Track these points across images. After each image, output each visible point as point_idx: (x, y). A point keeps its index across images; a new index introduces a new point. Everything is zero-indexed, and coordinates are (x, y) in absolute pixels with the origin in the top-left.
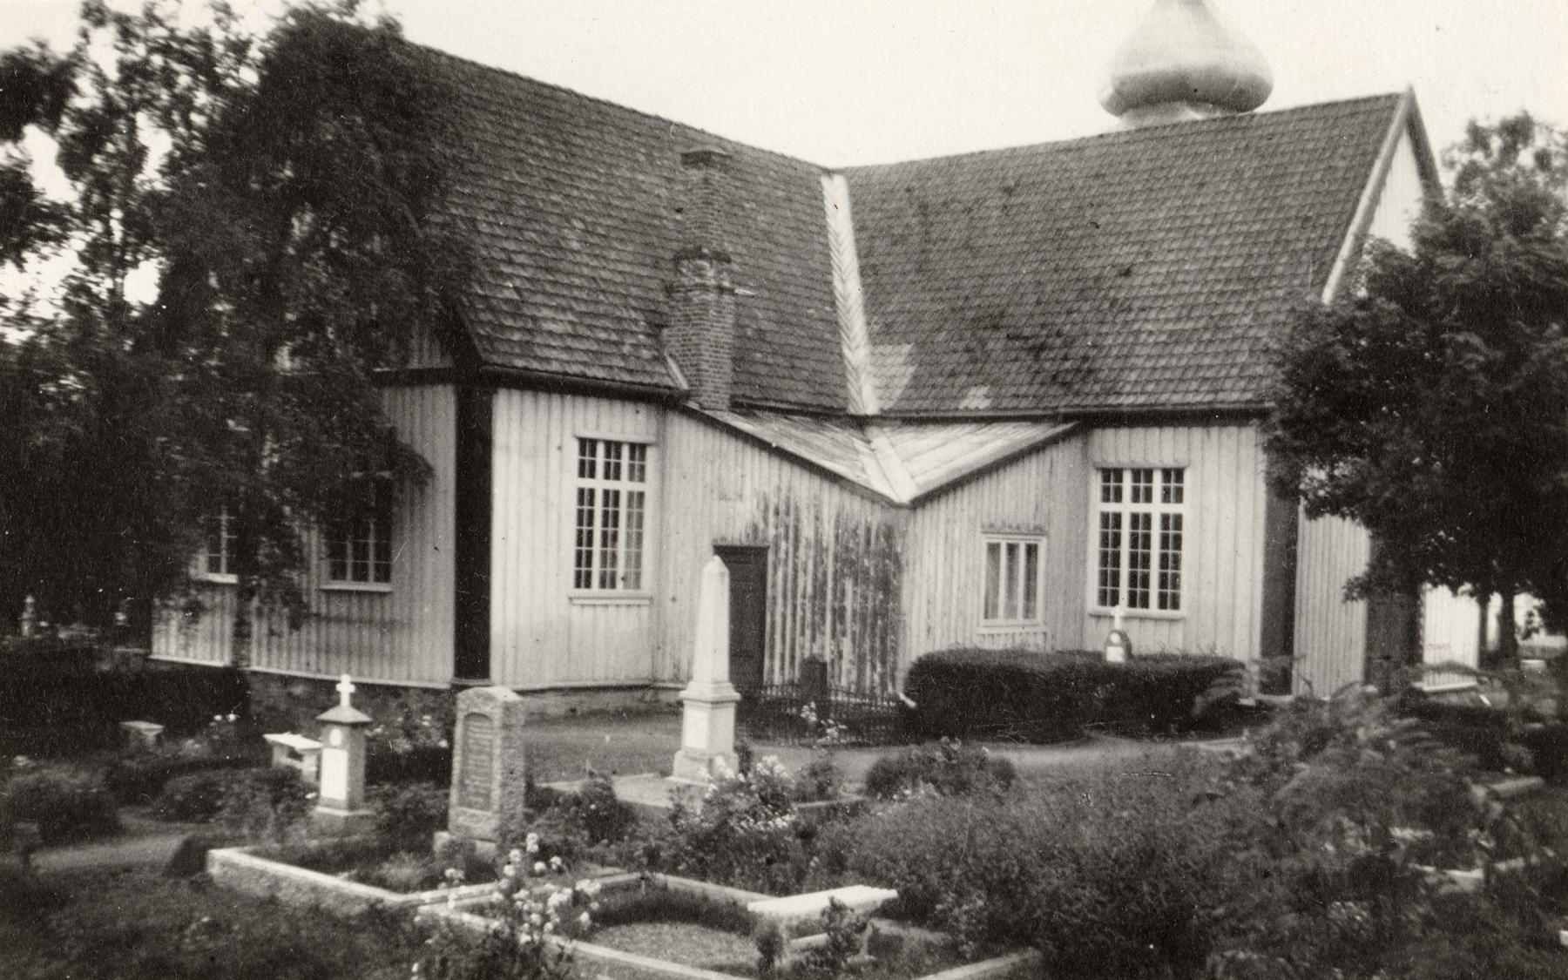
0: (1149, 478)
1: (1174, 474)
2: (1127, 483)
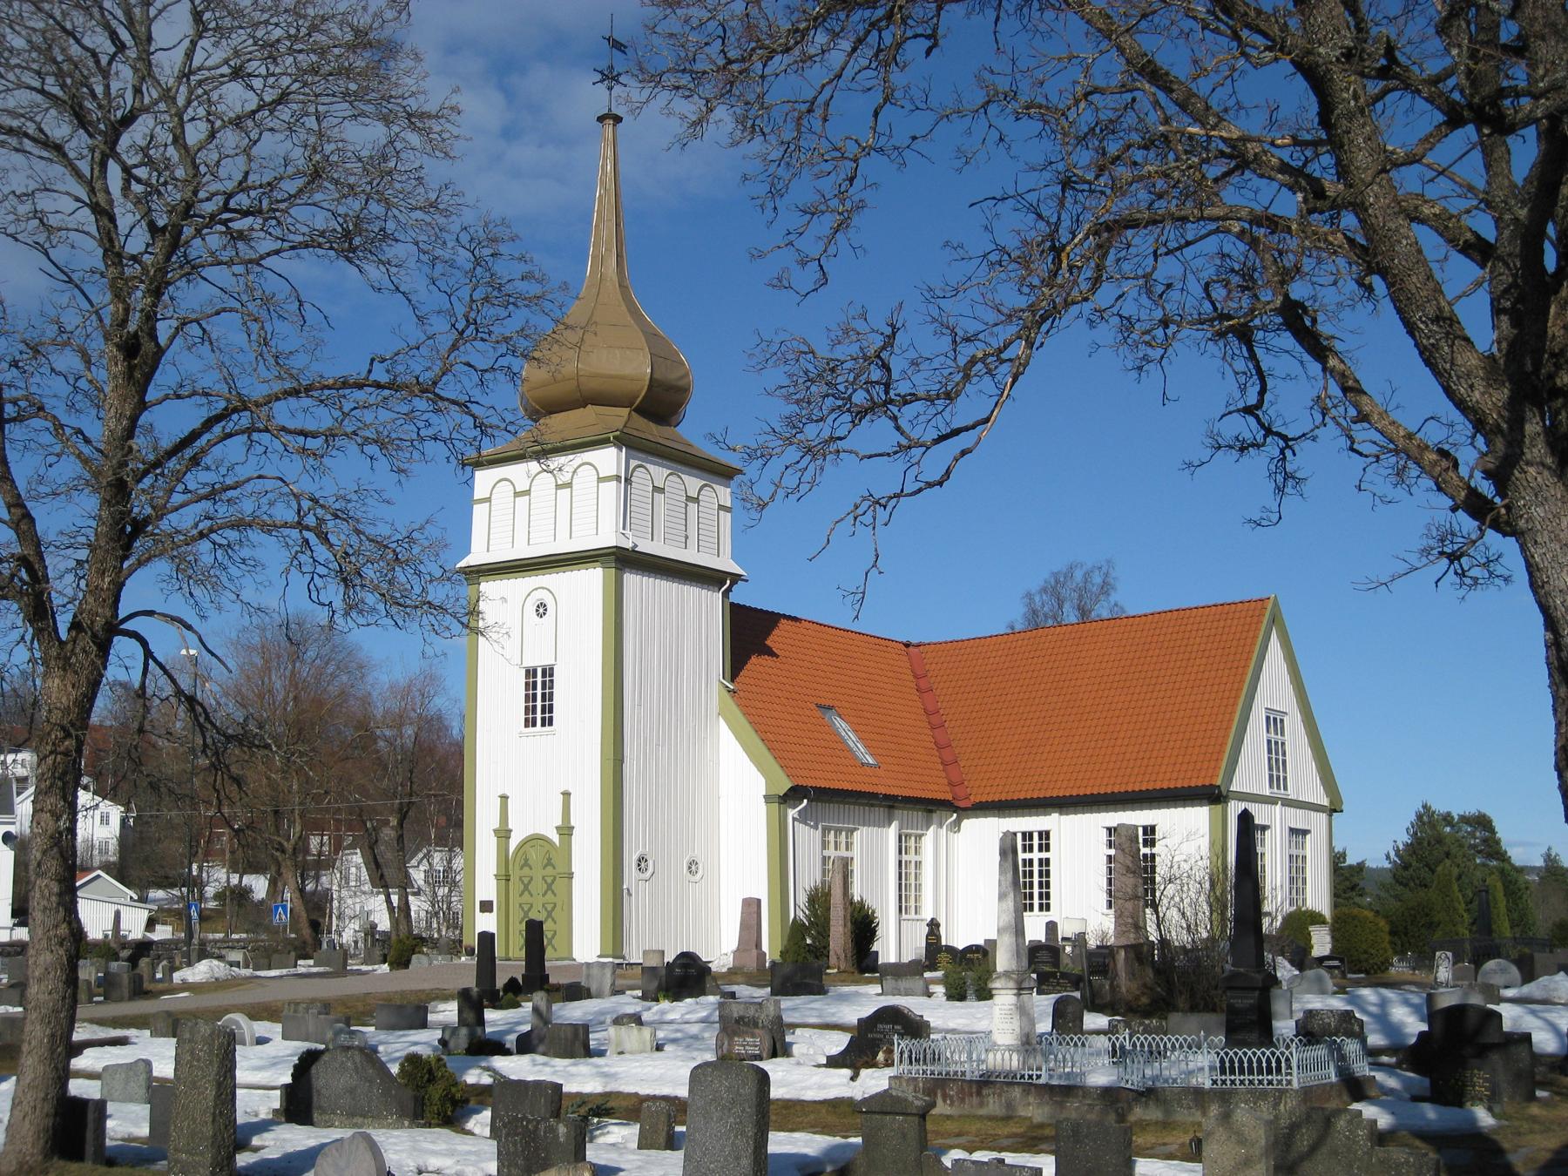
0: (1031, 838)
1: (1044, 836)
2: (1036, 842)
